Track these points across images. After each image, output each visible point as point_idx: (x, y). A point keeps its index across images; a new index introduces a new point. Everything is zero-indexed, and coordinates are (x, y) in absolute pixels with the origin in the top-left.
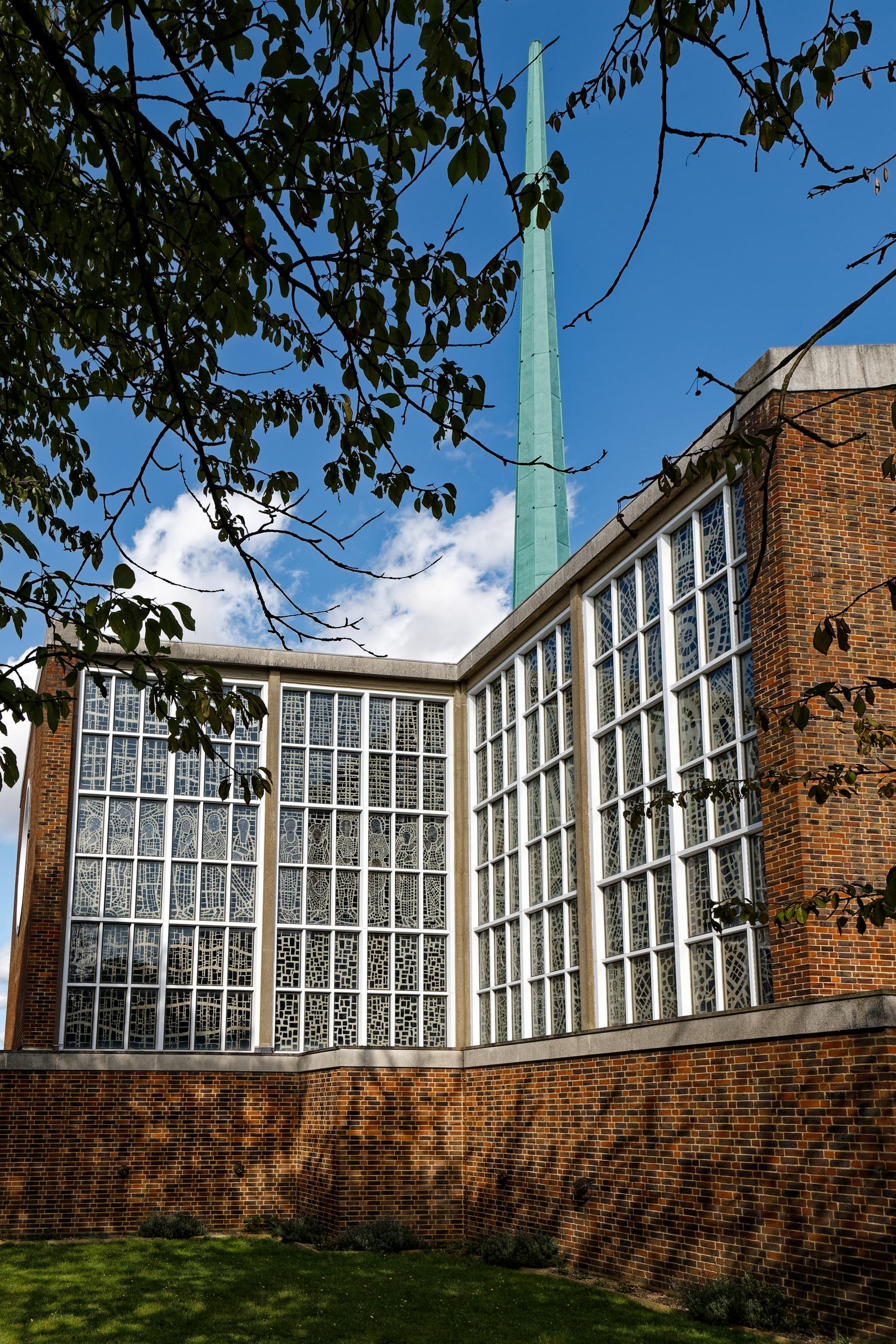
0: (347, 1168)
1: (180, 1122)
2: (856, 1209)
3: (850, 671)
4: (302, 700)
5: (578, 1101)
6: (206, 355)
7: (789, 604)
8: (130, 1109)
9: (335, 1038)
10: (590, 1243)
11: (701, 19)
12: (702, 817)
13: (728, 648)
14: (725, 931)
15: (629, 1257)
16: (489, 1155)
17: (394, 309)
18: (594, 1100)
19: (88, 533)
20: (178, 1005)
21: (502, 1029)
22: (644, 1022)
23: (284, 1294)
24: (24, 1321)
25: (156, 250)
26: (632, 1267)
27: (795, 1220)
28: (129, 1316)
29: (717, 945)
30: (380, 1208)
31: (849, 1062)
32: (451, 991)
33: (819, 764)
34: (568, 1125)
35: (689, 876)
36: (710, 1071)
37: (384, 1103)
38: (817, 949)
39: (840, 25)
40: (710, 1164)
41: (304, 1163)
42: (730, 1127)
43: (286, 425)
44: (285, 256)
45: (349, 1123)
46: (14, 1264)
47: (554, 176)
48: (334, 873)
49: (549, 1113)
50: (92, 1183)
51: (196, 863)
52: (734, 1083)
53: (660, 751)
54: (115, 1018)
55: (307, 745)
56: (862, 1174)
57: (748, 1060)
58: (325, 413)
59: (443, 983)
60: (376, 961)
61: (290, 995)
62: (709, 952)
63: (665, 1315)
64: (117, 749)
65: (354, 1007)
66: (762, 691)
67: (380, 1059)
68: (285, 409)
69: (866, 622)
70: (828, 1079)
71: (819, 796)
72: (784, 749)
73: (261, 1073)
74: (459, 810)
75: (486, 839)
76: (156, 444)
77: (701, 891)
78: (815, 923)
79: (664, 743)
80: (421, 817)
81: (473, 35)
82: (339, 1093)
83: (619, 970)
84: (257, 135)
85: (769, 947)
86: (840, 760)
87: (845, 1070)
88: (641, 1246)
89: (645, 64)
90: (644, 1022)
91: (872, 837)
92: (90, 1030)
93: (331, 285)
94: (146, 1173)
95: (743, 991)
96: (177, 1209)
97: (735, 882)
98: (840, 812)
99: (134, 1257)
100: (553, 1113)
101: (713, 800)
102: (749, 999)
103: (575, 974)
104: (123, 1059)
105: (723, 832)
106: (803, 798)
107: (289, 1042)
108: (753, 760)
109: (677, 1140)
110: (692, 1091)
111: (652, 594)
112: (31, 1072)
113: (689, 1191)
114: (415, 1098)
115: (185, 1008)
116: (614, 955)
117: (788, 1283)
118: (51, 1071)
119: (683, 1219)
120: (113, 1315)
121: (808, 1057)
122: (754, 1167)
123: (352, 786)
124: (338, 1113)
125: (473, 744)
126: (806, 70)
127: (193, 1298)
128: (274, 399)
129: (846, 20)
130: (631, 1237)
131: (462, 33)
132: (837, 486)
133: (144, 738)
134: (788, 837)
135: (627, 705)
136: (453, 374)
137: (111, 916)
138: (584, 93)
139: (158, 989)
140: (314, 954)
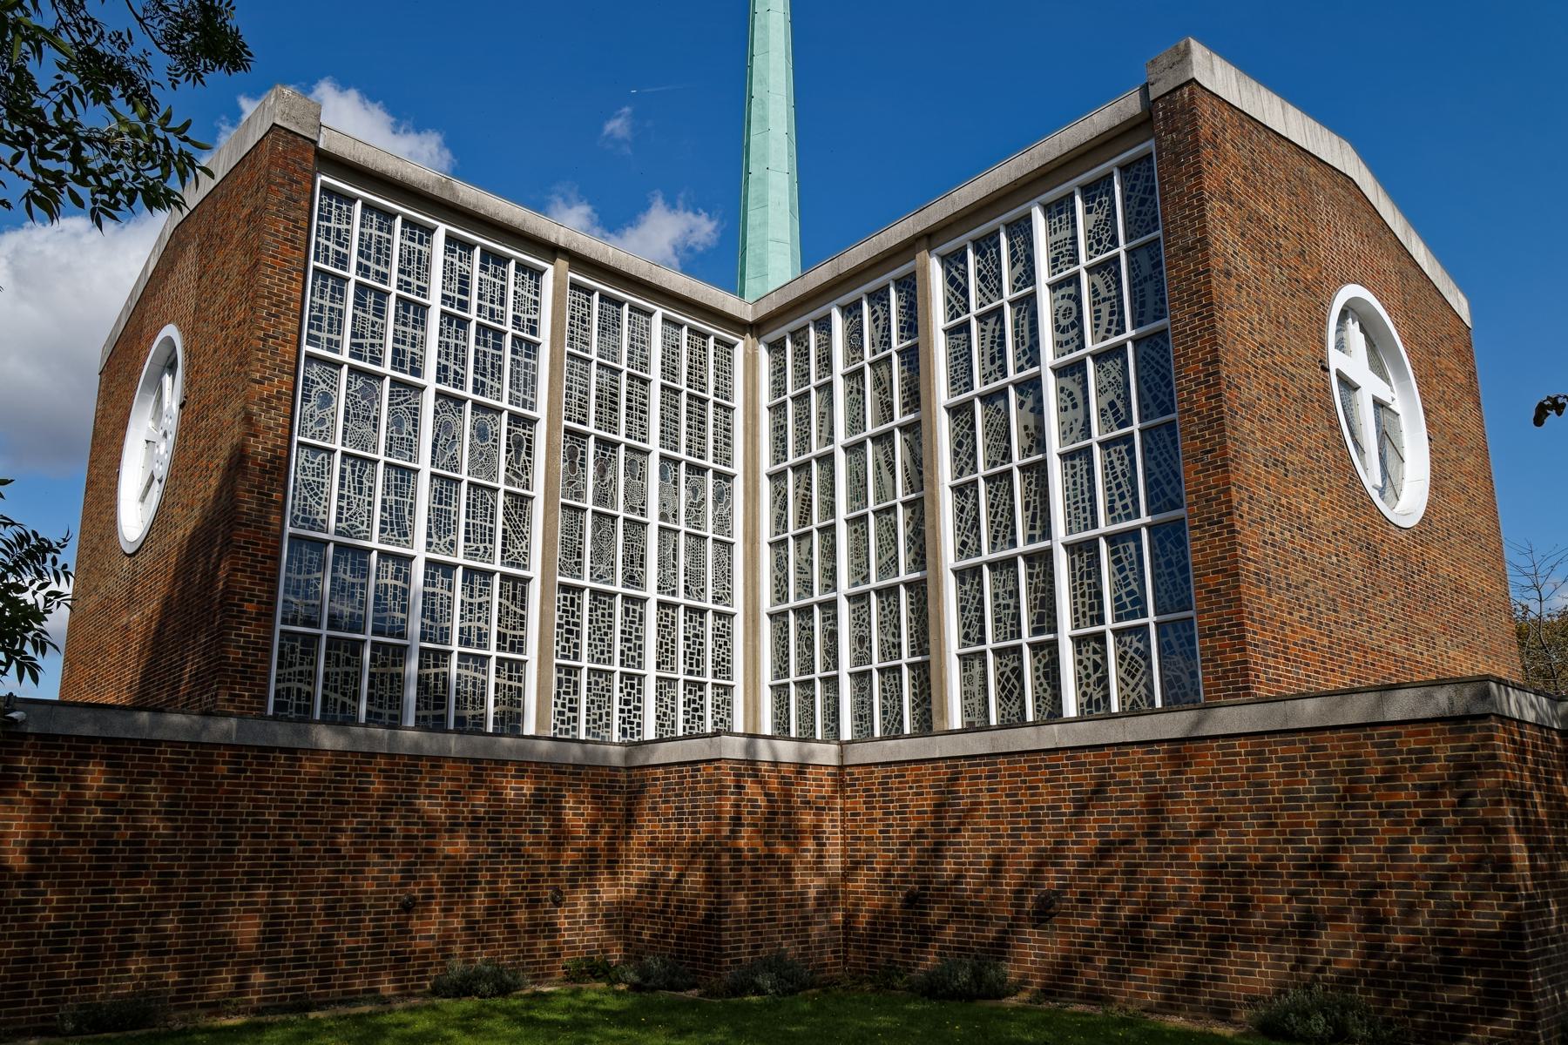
1: (483, 831)
8: (418, 811)
27: (1374, 920)
31: (1443, 751)
32: (738, 680)
36: (1242, 765)
45: (732, 831)
50: (363, 921)
54: (346, 682)
57: (1300, 750)
65: (639, 691)
67: (764, 752)
73: (582, 766)
87: (1437, 759)
105: (1114, 521)
112: (273, 749)
118: (305, 751)
121: (1387, 746)
139: (406, 647)
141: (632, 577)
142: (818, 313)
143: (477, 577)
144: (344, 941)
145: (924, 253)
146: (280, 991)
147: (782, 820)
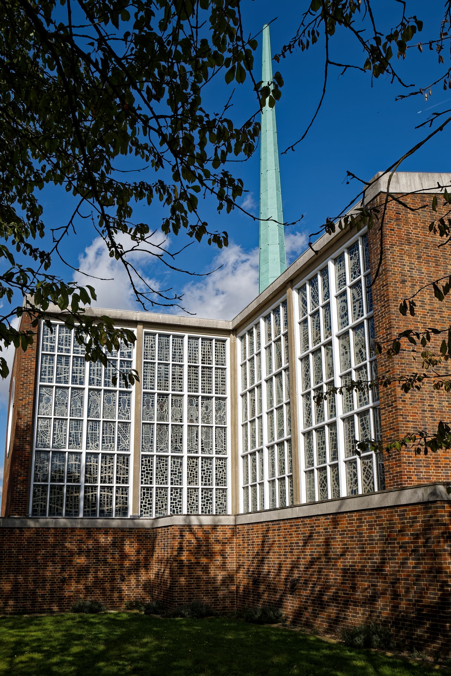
0: (177, 576)
2: (423, 589)
3: (419, 328)
4: (154, 338)
5: (292, 540)
6: (105, 164)
7: (391, 295)
8: (66, 547)
9: (171, 511)
10: (298, 610)
11: (344, 15)
12: (351, 398)
13: (362, 315)
14: (362, 455)
15: (316, 617)
16: (248, 568)
17: (199, 144)
18: (300, 540)
19: (44, 252)
20: (91, 494)
21: (255, 505)
22: (325, 500)
23: (145, 640)
24: (12, 656)
25: (82, 112)
26: (318, 621)
27: (396, 595)
28: (66, 653)
29: (359, 461)
30: (194, 596)
31: (421, 518)
32: (229, 486)
33: (406, 372)
34: (287, 552)
35: (345, 427)
37: (196, 543)
38: (405, 463)
39: (408, 22)
40: (355, 570)
41: (155, 574)
42: (364, 551)
43: (145, 199)
44: (145, 116)
45: (178, 553)
46: (6, 627)
47: (277, 83)
48: (170, 426)
49: (278, 547)
51: (100, 421)
52: (367, 529)
53: (331, 366)
54: (58, 501)
55: (157, 361)
56: (427, 572)
57: (373, 518)
58: (164, 194)
59: (225, 482)
60: (192, 471)
61: (148, 489)
62: (355, 465)
63: (333, 644)
64: (59, 362)
65: (180, 494)
66: (379, 337)
67: (194, 521)
68: (144, 191)
69: (426, 304)
70: (411, 526)
71: (406, 388)
72: (389, 365)
73: (133, 528)
74: (233, 395)
75: (246, 409)
76: (80, 205)
77: (351, 435)
78: (405, 451)
79: (333, 362)
80: (214, 398)
81: (237, 16)
82: (173, 538)
83: (312, 474)
84: (132, 57)
85: (383, 463)
86: (415, 371)
87: (419, 522)
88: (322, 611)
89: (318, 34)
90: (325, 500)
91: (431, 408)
92: (45, 507)
93: (168, 131)
94: (75, 580)
95: (371, 484)
96: (91, 598)
97: (367, 430)
98: (415, 396)
99: (69, 623)
100: (280, 547)
101: (356, 391)
102: (374, 488)
103: (290, 477)
104: (63, 521)
105: (361, 406)
106: (399, 389)
107: (147, 513)
108: (375, 371)
109: (340, 559)
110: (347, 534)
111: (326, 288)
112: (14, 528)
113: (346, 583)
114: (212, 540)
115: (94, 496)
116: (309, 467)
117: (391, 626)
118: (25, 528)
119: (342, 597)
120: (57, 653)
121: (402, 516)
122: (376, 570)
123: (179, 382)
124: (173, 548)
125: (239, 361)
126: (394, 42)
127: (99, 643)
128: (139, 186)
129: (411, 20)
130: (318, 607)
131: (232, 14)
132: (411, 239)
133: (73, 356)
134: (392, 408)
135: (315, 342)
136: (228, 178)
137: (56, 448)
138: (290, 46)
140: (160, 468)
141: (176, 448)
142: (255, 322)
143: (108, 457)
144: (40, 592)
145: (290, 289)
146: (18, 607)
147: (204, 548)
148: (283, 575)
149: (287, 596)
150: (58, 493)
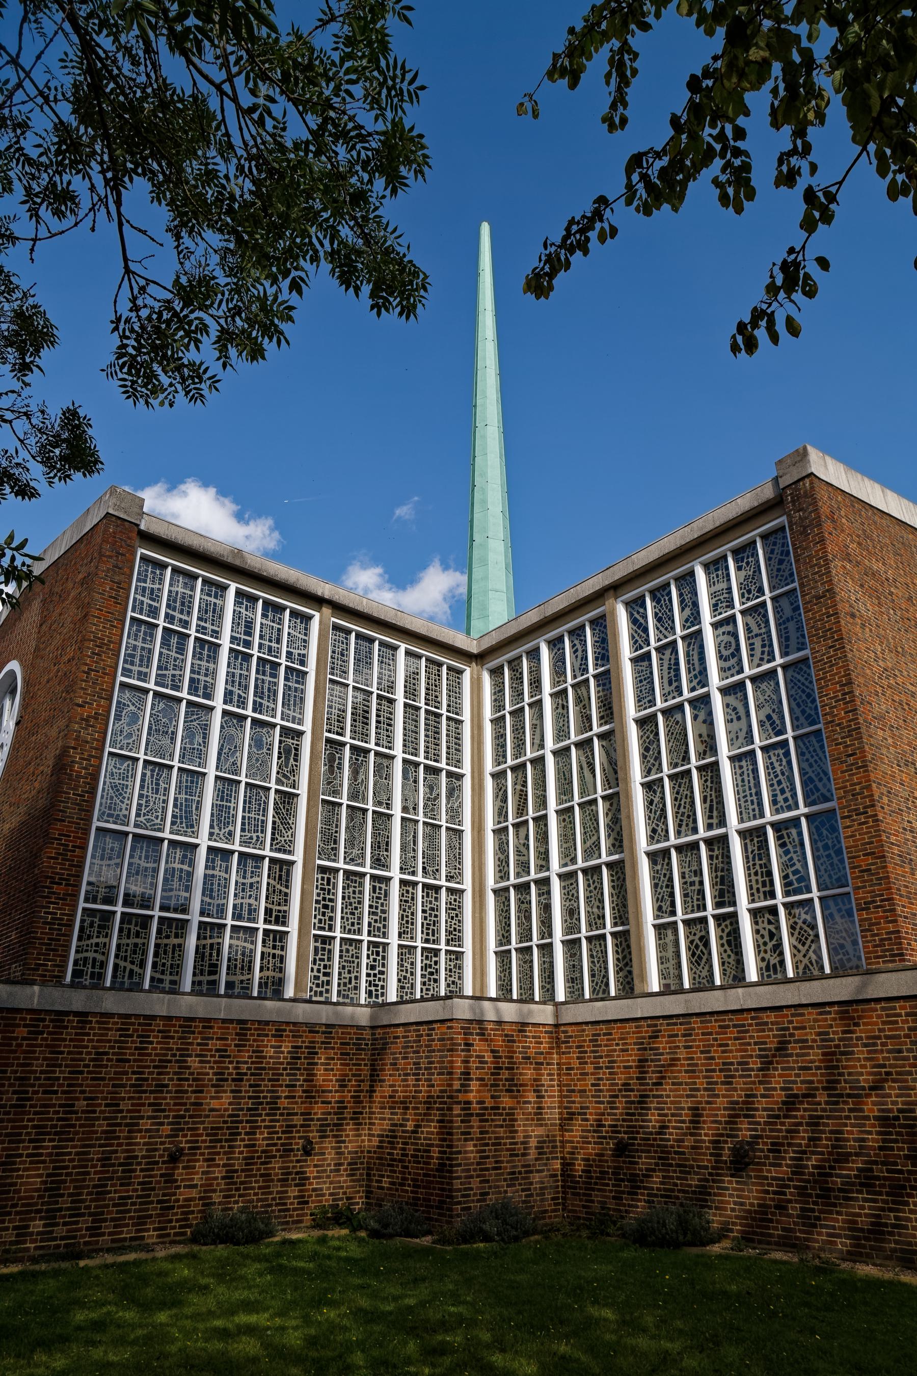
1: (245, 1086)
8: (189, 1068)
26: (821, 1237)
32: (468, 947)
54: (135, 952)
59: (460, 939)
64: (165, 643)
65: (384, 958)
92: (103, 965)
112: (67, 1013)
115: (216, 947)
119: (885, 1178)
130: (815, 1203)
141: (379, 860)
145: (611, 601)
148: (707, 1133)
149: (723, 1182)
150: (137, 935)
